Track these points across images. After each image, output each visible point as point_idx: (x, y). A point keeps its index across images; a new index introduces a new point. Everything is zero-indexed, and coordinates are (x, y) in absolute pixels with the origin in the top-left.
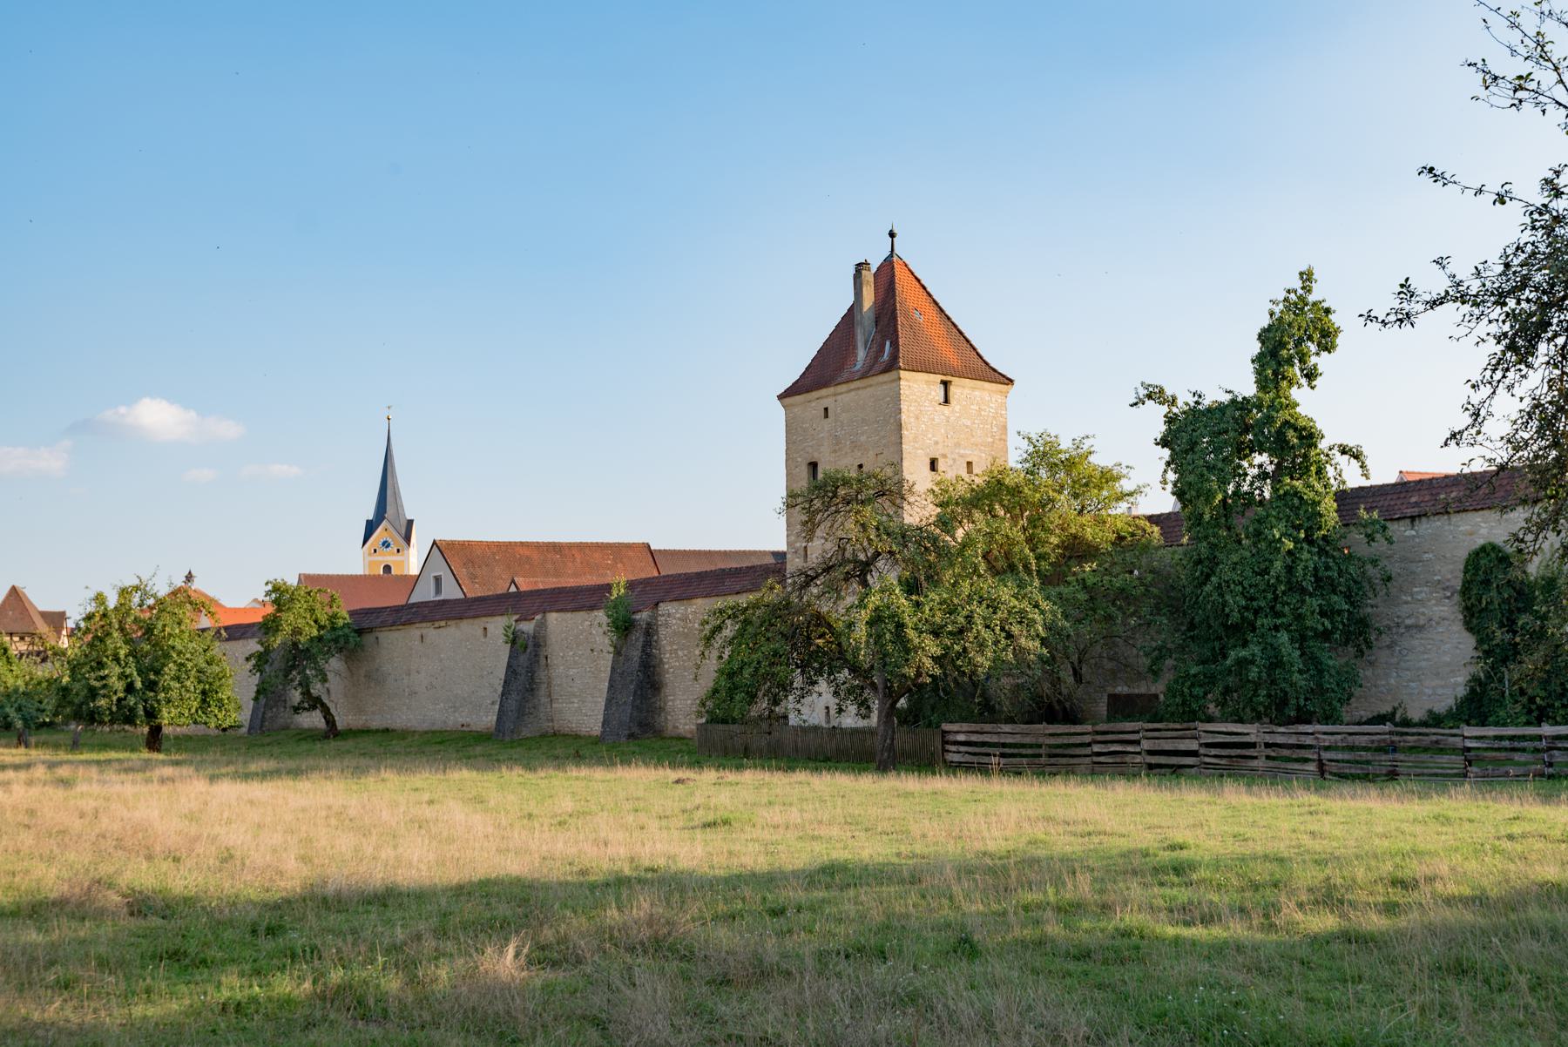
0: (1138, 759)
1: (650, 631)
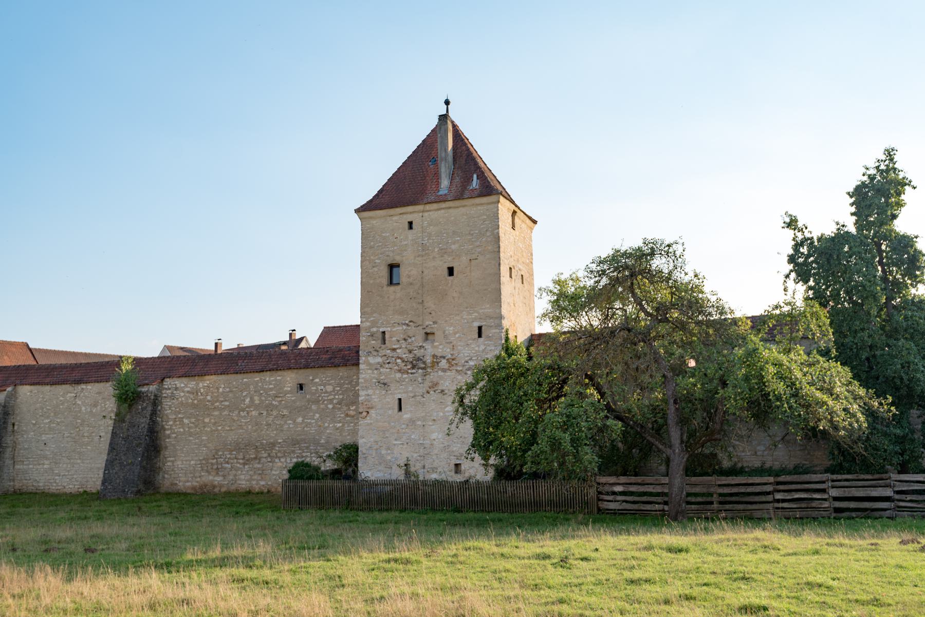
0: (826, 504)
1: (156, 402)
